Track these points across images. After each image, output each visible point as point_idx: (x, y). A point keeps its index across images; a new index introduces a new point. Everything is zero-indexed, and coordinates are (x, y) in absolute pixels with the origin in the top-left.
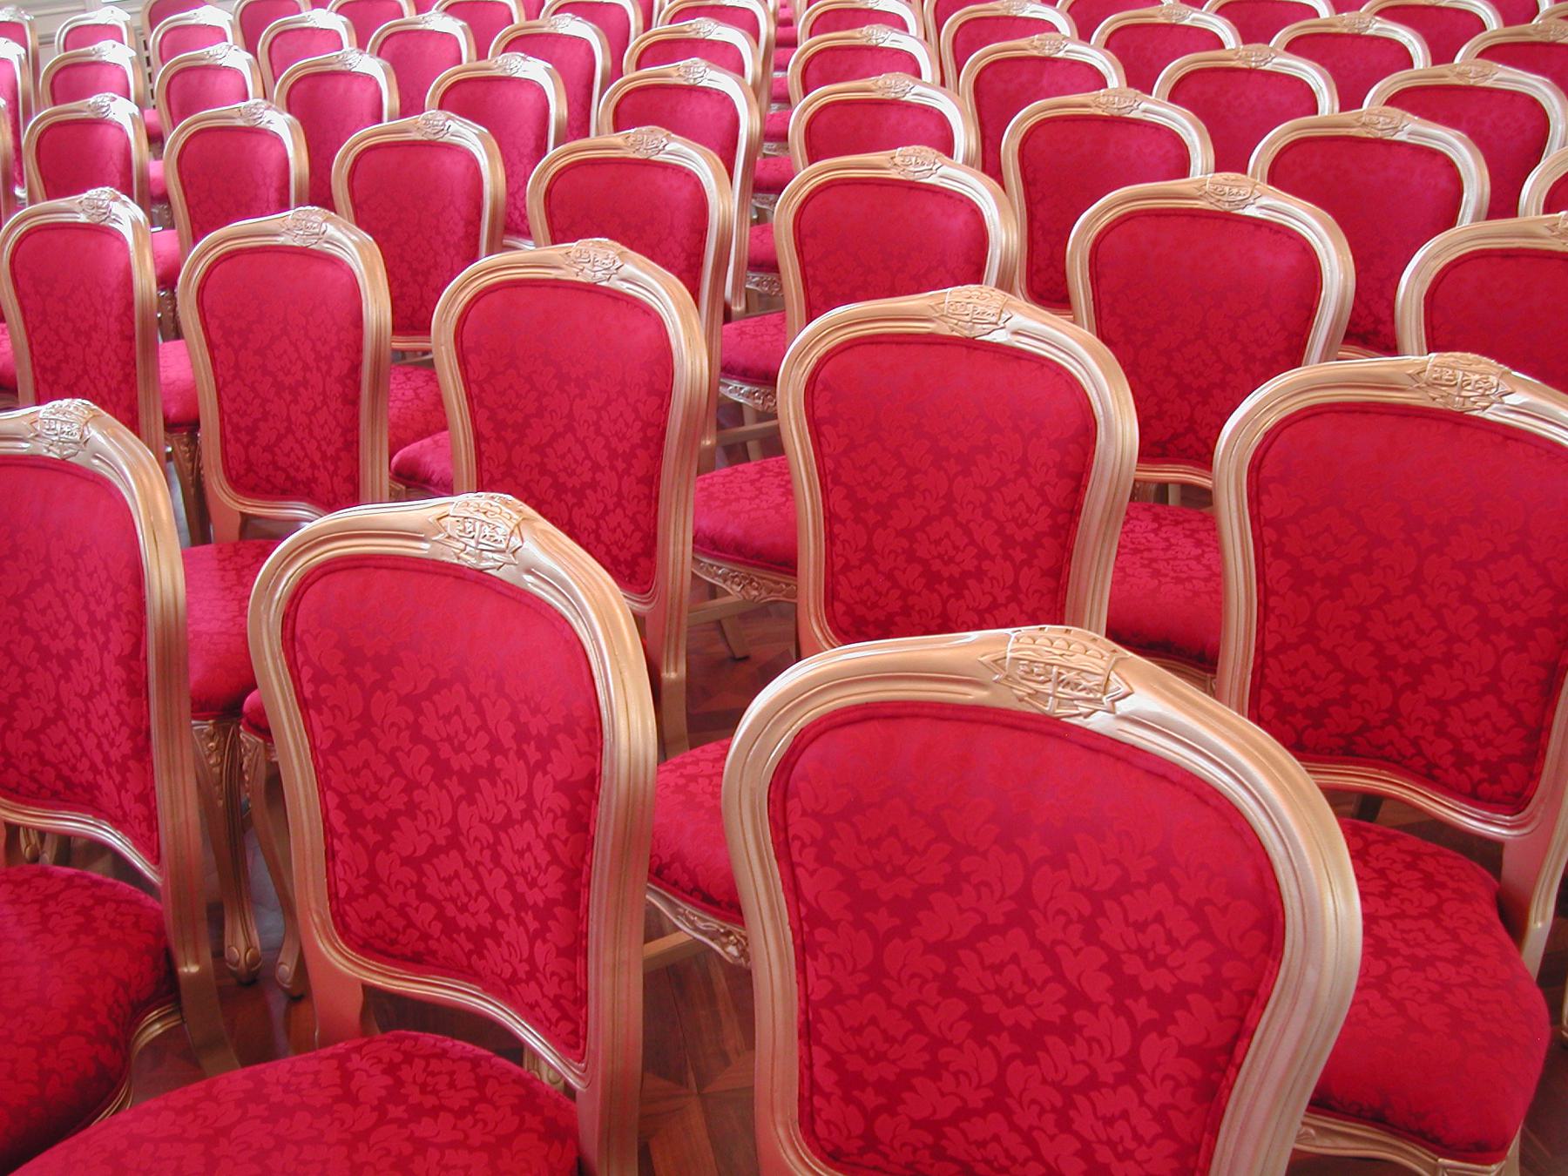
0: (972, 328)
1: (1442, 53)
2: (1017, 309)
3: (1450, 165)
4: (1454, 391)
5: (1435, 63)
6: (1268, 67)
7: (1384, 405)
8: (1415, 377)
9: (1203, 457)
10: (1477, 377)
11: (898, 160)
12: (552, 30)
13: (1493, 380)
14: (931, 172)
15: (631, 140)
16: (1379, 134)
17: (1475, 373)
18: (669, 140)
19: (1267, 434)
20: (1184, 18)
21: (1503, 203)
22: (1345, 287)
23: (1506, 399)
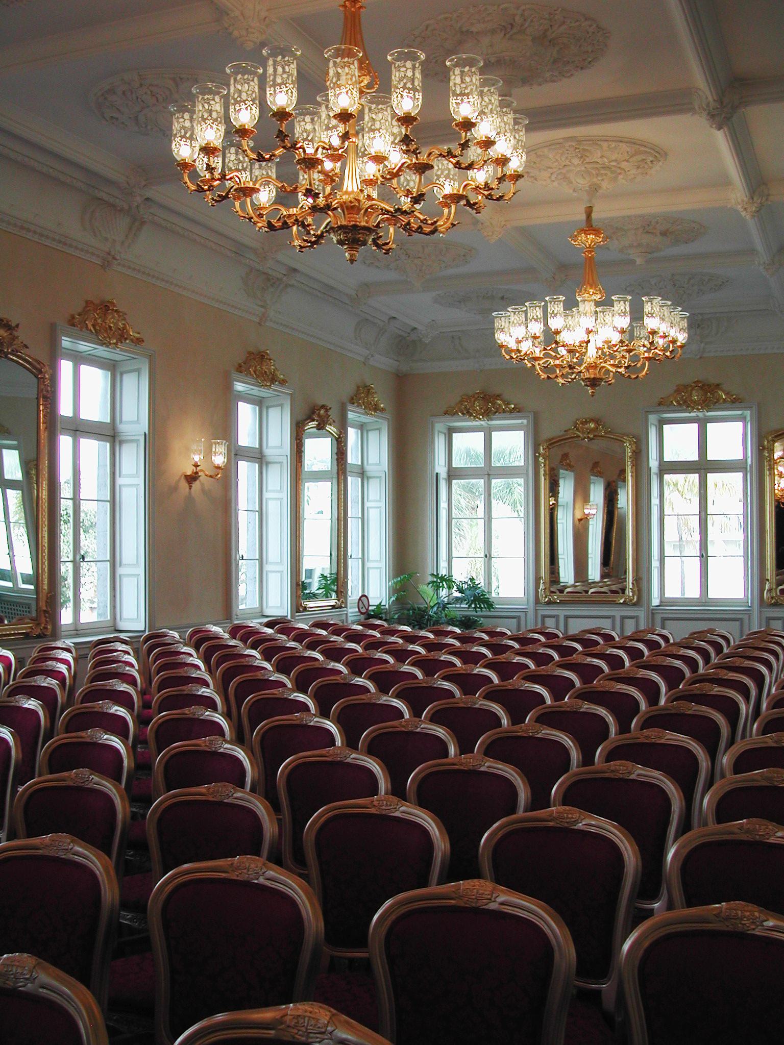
0: (476, 903)
1: (517, 718)
2: (502, 891)
3: (663, 791)
4: (738, 922)
5: (513, 725)
6: (539, 735)
7: (703, 931)
8: (717, 916)
9: (361, 941)
10: (748, 913)
11: (375, 803)
12: (100, 710)
13: (756, 914)
14: (396, 810)
15: (211, 790)
16: (621, 776)
17: (747, 911)
18: (236, 791)
19: (646, 951)
20: (475, 704)
21: (540, 800)
22: (637, 865)
23: (765, 924)
